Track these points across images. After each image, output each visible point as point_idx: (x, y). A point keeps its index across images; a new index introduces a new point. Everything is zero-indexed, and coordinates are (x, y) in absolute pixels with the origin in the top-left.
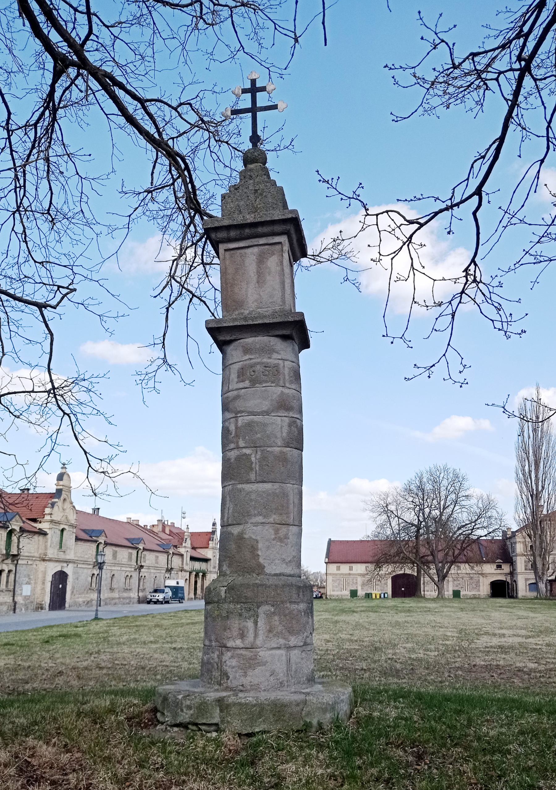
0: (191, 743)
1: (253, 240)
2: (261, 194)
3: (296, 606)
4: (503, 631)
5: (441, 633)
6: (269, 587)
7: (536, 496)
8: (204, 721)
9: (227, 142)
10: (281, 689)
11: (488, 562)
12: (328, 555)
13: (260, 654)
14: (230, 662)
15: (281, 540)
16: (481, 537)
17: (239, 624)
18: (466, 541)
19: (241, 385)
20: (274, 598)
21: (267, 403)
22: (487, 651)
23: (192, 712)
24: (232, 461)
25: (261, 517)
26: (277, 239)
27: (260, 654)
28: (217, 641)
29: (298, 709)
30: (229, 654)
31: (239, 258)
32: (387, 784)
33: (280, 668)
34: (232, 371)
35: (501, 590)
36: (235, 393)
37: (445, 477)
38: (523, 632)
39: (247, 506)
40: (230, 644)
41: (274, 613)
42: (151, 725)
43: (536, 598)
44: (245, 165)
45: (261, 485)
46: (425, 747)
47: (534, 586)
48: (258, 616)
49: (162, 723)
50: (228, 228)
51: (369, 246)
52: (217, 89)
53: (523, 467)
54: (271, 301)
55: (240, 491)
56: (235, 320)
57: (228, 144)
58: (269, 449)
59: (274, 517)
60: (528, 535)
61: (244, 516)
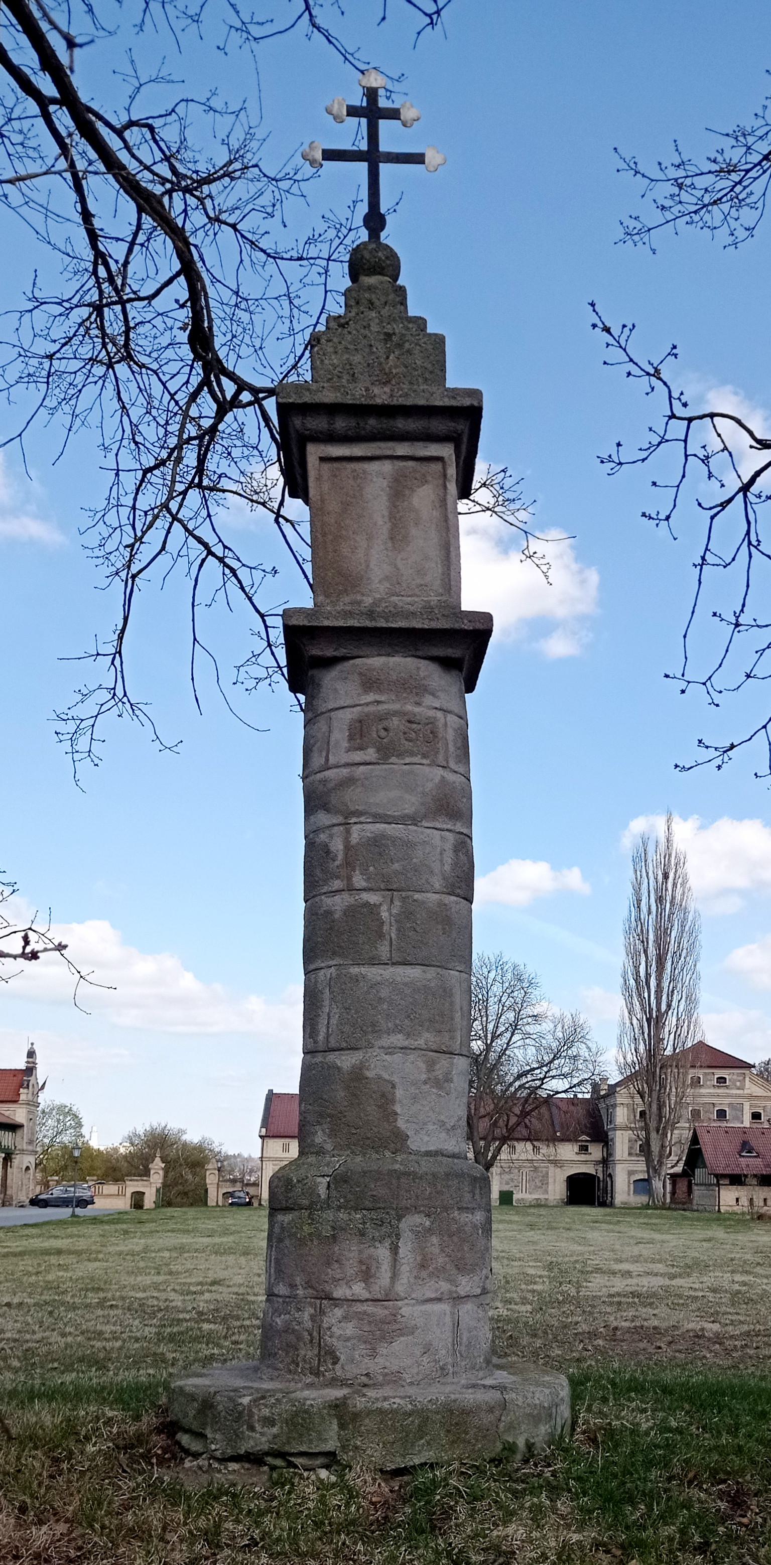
0: (290, 1493)
1: (382, 445)
2: (400, 346)
3: (470, 1216)
4: (625, 1266)
5: (516, 1270)
6: (421, 1178)
7: (655, 1021)
8: (304, 1448)
9: (234, 226)
10: (442, 1380)
11: (563, 1140)
12: (265, 1123)
13: (403, 1311)
14: (340, 1328)
15: (438, 1084)
16: (558, 1093)
17: (360, 1252)
18: (531, 1101)
19: (358, 757)
20: (430, 1198)
21: (413, 799)
22: (617, 1301)
23: (275, 1430)
24: (337, 916)
25: (400, 1036)
26: (434, 450)
27: (403, 1311)
28: (308, 1285)
29: (491, 1417)
30: (339, 1312)
31: (351, 482)
32: (705, 1552)
33: (441, 1337)
34: (335, 724)
35: (585, 1191)
36: (345, 771)
37: (499, 978)
38: (660, 1268)
39: (372, 1012)
40: (338, 1293)
41: (430, 1230)
42: (169, 1460)
43: (647, 1207)
44: (354, 277)
45: (400, 969)
46: (738, 1483)
47: (643, 1185)
48: (398, 1237)
49: (196, 1455)
50: (333, 410)
51: (654, 484)
52: (216, 103)
53: (637, 968)
54: (419, 581)
55: (356, 979)
56: (350, 614)
57: (236, 230)
58: (417, 896)
59: (426, 1038)
60: (639, 1092)
61: (365, 1033)
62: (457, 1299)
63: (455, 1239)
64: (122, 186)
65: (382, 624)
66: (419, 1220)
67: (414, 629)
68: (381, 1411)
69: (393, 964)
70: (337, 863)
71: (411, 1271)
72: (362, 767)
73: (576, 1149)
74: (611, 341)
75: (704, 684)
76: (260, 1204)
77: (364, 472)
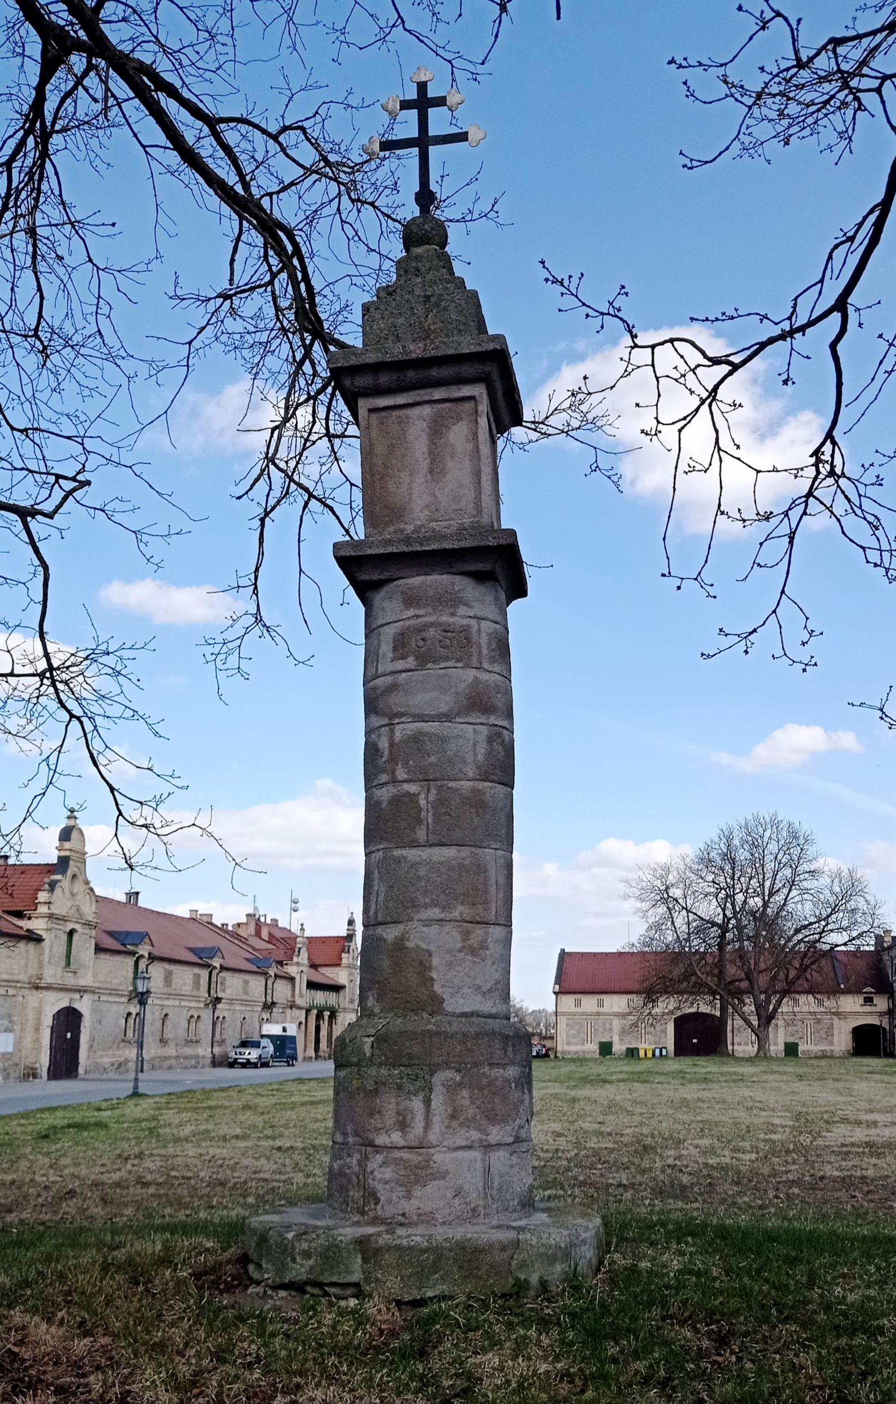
0: (311, 1318)
1: (422, 392)
2: (437, 305)
3: (502, 1071)
5: (762, 1120)
8: (334, 1279)
9: (372, 204)
10: (474, 1221)
11: (844, 992)
12: (559, 979)
13: (435, 1158)
14: (381, 1173)
15: (473, 951)
16: (837, 946)
18: (810, 954)
19: (400, 665)
20: (460, 1056)
21: (448, 699)
24: (384, 805)
25: (436, 910)
26: (466, 391)
28: (356, 1134)
29: (504, 1256)
30: (379, 1158)
33: (472, 1182)
34: (383, 638)
36: (389, 679)
39: (412, 889)
40: (381, 1140)
41: (460, 1085)
42: (237, 1286)
44: (407, 247)
45: (436, 850)
46: (732, 1324)
48: (431, 1090)
49: (258, 1283)
50: (376, 368)
51: (637, 405)
52: (352, 100)
54: (454, 507)
55: (399, 860)
56: (389, 542)
57: (375, 207)
59: (460, 911)
61: (406, 908)
62: (487, 1147)
63: (485, 1092)
64: (222, 199)
65: (417, 548)
66: (450, 1076)
67: (445, 550)
68: (399, 1248)
69: (431, 846)
70: (384, 759)
71: (442, 1121)
72: (403, 675)
73: (862, 1001)
74: (565, 291)
75: (696, 579)
76: (556, 1057)
77: (407, 417)
